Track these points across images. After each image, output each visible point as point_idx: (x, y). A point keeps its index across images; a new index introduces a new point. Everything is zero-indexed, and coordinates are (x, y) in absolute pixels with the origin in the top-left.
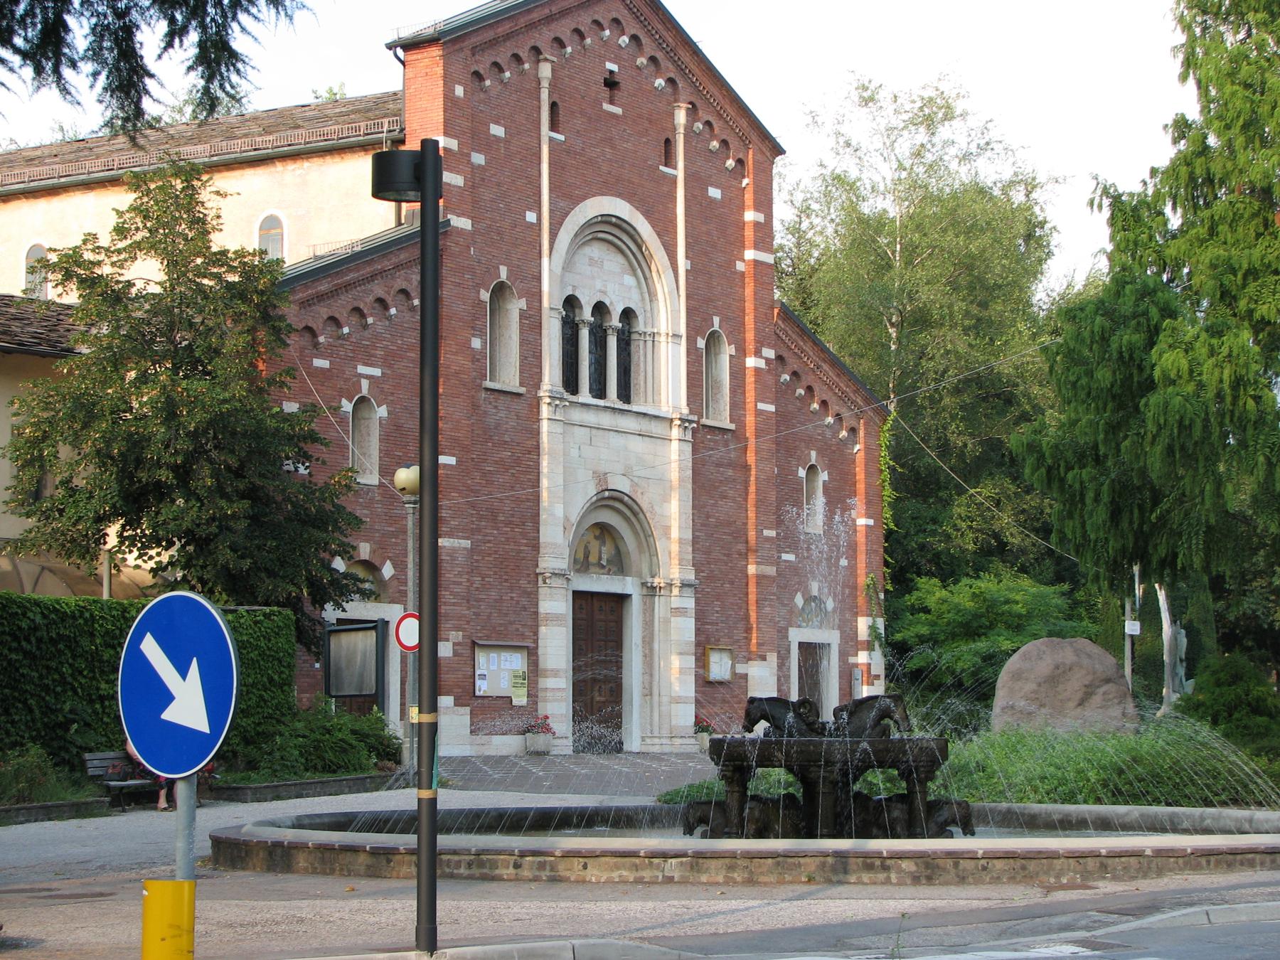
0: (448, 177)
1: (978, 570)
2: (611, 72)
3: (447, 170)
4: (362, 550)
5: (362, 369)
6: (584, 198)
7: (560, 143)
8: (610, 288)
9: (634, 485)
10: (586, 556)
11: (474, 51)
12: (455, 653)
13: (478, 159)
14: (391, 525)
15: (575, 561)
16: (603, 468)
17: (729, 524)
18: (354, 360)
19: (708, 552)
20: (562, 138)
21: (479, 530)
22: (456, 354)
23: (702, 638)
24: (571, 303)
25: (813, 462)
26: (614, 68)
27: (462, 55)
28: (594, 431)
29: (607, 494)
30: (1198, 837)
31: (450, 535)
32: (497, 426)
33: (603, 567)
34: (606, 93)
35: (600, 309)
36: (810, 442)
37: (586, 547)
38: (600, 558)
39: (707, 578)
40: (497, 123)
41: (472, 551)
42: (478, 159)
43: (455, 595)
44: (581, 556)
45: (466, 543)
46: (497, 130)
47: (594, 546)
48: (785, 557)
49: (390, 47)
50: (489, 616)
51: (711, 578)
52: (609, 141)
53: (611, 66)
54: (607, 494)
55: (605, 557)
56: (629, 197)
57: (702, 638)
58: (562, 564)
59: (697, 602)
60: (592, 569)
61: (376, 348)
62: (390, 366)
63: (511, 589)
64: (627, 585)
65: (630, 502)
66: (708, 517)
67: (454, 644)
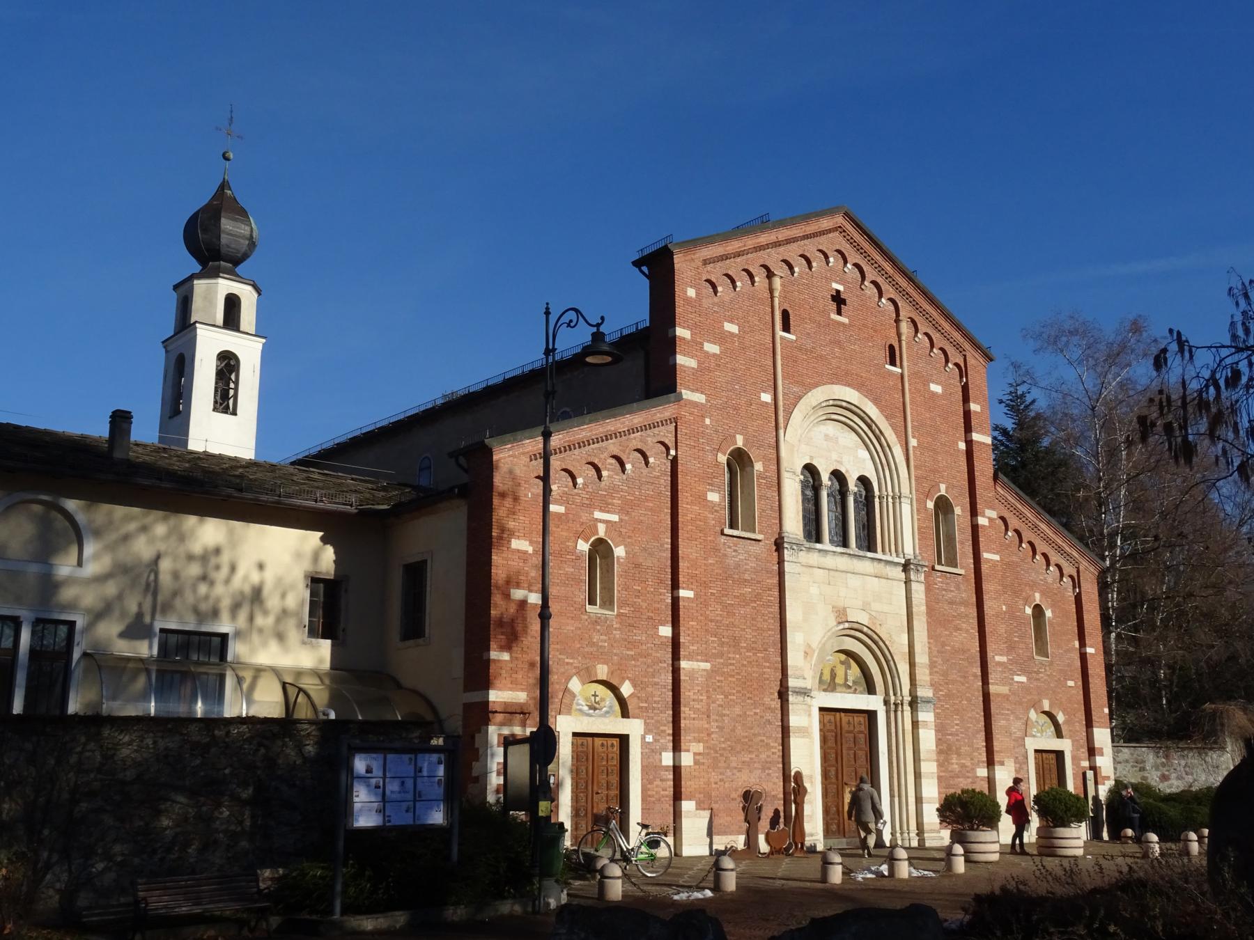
0: (681, 359)
1: (1184, 799)
2: (838, 292)
3: (681, 353)
4: (599, 671)
5: (598, 515)
6: (816, 385)
7: (791, 341)
8: (845, 459)
9: (872, 618)
10: (833, 675)
11: (706, 262)
12: (696, 762)
13: (712, 348)
14: (628, 649)
15: (821, 681)
16: (841, 604)
17: (964, 652)
18: (591, 507)
19: (945, 674)
20: (793, 337)
21: (721, 655)
22: (692, 503)
23: (944, 747)
24: (810, 470)
25: (1038, 602)
26: (841, 288)
27: (693, 265)
28: (832, 573)
29: (847, 625)
30: (1095, 596)
31: (690, 658)
32: (738, 566)
33: (850, 687)
34: (834, 306)
35: (837, 475)
36: (1033, 586)
37: (832, 670)
38: (846, 680)
39: (946, 696)
40: (731, 321)
41: (710, 674)
42: (712, 348)
43: (696, 711)
44: (827, 677)
45: (707, 666)
46: (731, 328)
47: (840, 671)
48: (1017, 678)
49: (638, 264)
50: (733, 730)
51: (949, 696)
52: (838, 343)
53: (836, 286)
54: (847, 625)
55: (851, 679)
56: (859, 387)
57: (944, 747)
58: (809, 682)
59: (937, 716)
60: (839, 689)
61: (614, 498)
62: (628, 513)
63: (755, 705)
64: (874, 703)
65: (870, 632)
66: (944, 644)
67: (695, 754)
